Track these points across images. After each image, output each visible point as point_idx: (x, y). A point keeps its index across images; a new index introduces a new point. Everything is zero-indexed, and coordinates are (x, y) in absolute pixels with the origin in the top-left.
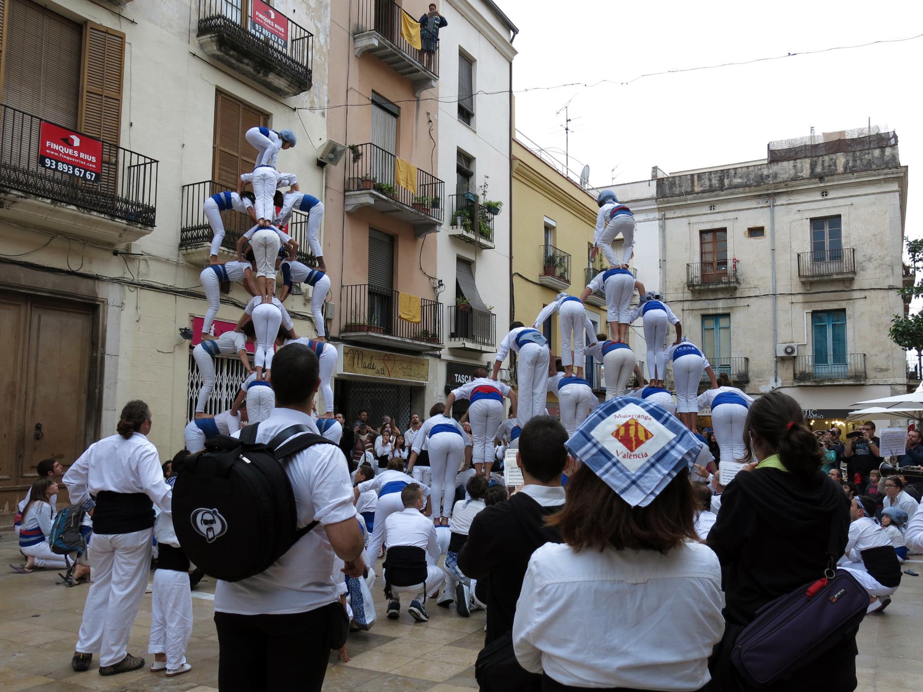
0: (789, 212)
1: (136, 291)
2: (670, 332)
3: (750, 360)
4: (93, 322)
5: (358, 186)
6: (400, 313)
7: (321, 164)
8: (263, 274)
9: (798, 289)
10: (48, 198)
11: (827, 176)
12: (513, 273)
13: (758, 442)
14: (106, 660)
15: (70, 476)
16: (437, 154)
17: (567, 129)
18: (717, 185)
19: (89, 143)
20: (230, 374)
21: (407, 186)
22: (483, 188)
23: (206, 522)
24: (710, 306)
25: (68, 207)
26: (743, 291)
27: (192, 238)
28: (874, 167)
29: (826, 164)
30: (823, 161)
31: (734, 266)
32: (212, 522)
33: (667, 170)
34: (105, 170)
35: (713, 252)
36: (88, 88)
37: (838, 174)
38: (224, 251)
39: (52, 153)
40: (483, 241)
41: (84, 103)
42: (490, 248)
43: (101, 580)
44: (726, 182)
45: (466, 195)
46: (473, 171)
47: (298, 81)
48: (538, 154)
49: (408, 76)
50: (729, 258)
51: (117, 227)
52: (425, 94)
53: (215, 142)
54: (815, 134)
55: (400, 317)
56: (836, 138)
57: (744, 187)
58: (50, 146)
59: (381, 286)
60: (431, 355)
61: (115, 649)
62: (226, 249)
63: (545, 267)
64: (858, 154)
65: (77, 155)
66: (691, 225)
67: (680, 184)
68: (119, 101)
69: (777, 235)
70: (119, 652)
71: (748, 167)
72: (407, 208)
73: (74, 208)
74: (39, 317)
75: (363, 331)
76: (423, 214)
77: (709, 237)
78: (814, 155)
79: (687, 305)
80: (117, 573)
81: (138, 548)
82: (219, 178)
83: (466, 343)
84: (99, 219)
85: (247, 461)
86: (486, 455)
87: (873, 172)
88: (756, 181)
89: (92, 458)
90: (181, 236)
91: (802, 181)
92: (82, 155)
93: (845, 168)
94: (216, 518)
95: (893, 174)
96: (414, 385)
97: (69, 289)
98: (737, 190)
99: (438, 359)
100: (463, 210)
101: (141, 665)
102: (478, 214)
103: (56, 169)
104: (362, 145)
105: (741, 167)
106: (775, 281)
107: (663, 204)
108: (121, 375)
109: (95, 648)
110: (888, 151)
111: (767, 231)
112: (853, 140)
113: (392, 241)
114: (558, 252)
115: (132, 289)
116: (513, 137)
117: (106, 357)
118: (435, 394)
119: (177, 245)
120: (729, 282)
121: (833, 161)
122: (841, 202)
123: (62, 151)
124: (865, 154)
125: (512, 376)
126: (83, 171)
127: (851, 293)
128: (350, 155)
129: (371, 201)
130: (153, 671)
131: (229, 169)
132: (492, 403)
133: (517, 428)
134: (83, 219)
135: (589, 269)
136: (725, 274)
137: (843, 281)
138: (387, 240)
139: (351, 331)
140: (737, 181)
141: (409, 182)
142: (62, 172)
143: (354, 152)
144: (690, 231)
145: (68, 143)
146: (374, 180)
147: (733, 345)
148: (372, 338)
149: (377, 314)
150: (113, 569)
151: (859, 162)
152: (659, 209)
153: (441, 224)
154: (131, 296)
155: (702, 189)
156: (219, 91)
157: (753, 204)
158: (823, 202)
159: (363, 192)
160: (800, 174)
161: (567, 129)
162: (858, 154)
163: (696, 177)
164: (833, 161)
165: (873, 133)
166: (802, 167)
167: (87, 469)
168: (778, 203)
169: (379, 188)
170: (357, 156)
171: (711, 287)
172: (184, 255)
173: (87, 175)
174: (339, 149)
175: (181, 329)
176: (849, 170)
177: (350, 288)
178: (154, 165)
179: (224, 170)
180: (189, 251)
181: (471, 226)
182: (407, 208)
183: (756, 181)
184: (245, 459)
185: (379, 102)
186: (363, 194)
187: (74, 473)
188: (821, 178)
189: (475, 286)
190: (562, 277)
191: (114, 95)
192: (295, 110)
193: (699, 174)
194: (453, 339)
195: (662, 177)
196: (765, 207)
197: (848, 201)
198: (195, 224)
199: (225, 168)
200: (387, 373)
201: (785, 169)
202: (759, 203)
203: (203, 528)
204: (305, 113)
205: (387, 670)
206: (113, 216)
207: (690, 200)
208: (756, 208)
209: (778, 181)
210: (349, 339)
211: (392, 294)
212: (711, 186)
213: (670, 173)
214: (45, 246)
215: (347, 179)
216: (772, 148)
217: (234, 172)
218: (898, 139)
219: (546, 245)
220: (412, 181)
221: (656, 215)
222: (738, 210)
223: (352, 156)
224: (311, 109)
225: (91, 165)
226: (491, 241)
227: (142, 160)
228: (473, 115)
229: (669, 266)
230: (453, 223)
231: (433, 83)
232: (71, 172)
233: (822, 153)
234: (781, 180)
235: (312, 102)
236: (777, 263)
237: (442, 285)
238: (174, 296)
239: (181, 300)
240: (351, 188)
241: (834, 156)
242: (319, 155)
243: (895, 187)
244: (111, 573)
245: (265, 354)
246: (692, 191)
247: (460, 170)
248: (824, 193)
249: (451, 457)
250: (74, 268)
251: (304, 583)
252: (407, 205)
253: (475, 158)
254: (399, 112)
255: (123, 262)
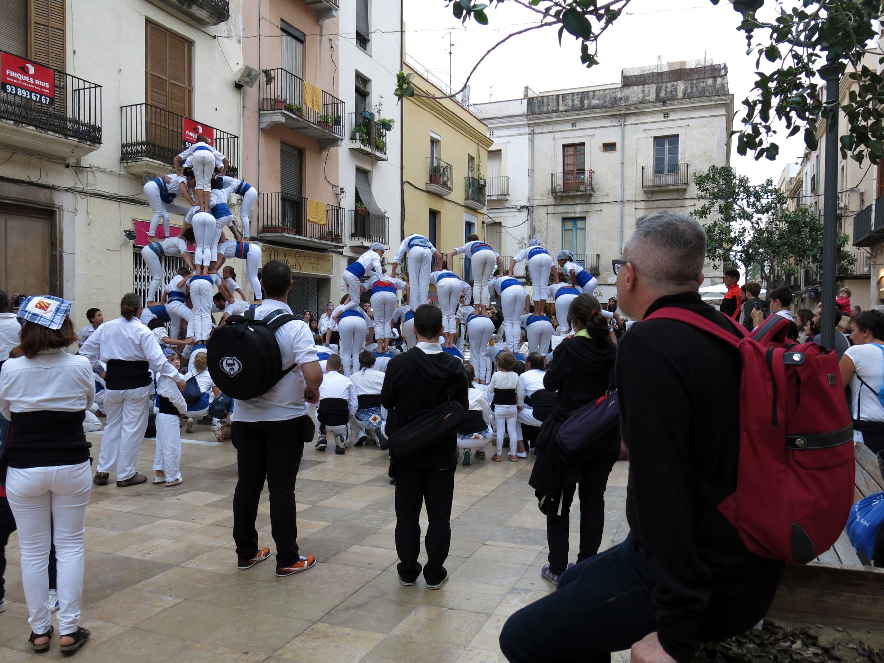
0: (636, 130)
1: (86, 199)
2: (536, 232)
3: (601, 256)
4: (51, 225)
5: (271, 106)
6: (309, 217)
7: (238, 86)
8: (201, 188)
9: (641, 197)
10: (11, 120)
11: (669, 100)
12: (404, 181)
13: (576, 323)
14: (122, 477)
15: (85, 349)
16: (338, 76)
17: (450, 53)
18: (579, 105)
19: (43, 71)
20: (167, 269)
21: (313, 106)
22: (378, 106)
23: (229, 365)
24: (570, 210)
25: (28, 127)
26: (597, 197)
27: (132, 153)
28: (707, 94)
29: (669, 90)
30: (666, 87)
31: (591, 176)
32: (233, 365)
33: (537, 90)
34: (57, 94)
35: (574, 164)
36: (35, 19)
37: (678, 99)
38: (160, 164)
39: (12, 80)
40: (378, 154)
41: (33, 33)
42: (385, 160)
43: (113, 423)
44: (586, 102)
45: (364, 114)
46: (369, 91)
47: (217, 13)
48: (425, 75)
49: (312, 6)
50: (586, 169)
51: (70, 144)
52: (327, 23)
53: (146, 67)
54: (662, 64)
55: (309, 220)
56: (678, 67)
57: (601, 107)
58: (9, 74)
59: (292, 192)
60: (335, 252)
61: (129, 468)
62: (162, 163)
63: (431, 176)
64: (695, 82)
65: (33, 82)
66: (556, 139)
67: (547, 103)
68: (63, 31)
69: (626, 151)
70: (131, 471)
71: (604, 90)
72: (314, 125)
73: (33, 128)
74: (6, 220)
75: (278, 232)
76: (327, 131)
77: (571, 151)
78: (659, 81)
79: (550, 209)
80: (127, 417)
81: (142, 399)
82: (152, 100)
83: (364, 242)
84: (54, 137)
85: (253, 330)
86: (385, 333)
87: (706, 98)
88: (610, 103)
89: (103, 336)
90: (122, 151)
91: (649, 104)
92: (37, 82)
93: (684, 94)
94: (235, 362)
95: (722, 100)
96: (321, 277)
97: (30, 198)
98: (595, 110)
99: (341, 256)
100: (360, 126)
101: (145, 481)
102: (374, 130)
103: (16, 95)
104: (273, 70)
105: (599, 90)
106: (623, 189)
107: (532, 120)
108: (78, 270)
109: (112, 469)
110: (719, 80)
111: (618, 146)
112: (691, 70)
113: (300, 154)
114: (442, 163)
115: (83, 197)
116: (404, 61)
117: (65, 255)
118: (338, 285)
119: (119, 159)
120: (586, 190)
121: (675, 87)
122: (679, 123)
123: (20, 78)
124: (700, 83)
125: (403, 269)
126: (39, 96)
127: (684, 201)
128: (263, 78)
129: (283, 120)
130: (155, 484)
131: (159, 91)
132: (388, 294)
133: (411, 312)
134: (41, 138)
135: (469, 178)
136: (583, 183)
137: (677, 191)
138: (296, 153)
139: (268, 232)
140: (595, 102)
141: (315, 102)
142: (21, 97)
143: (267, 76)
144: (555, 144)
145: (25, 71)
146: (285, 100)
147: (587, 243)
148: (285, 238)
149: (289, 218)
150: (123, 412)
151: (695, 89)
152: (529, 125)
153: (342, 140)
154: (82, 203)
155: (566, 108)
156: (148, 21)
157: (607, 123)
158: (665, 123)
159: (276, 111)
160: (647, 98)
161: (450, 53)
162: (695, 82)
163: (561, 97)
164: (675, 87)
165: (708, 64)
166: (649, 91)
167: (99, 344)
168: (628, 122)
169: (289, 108)
170: (270, 79)
171: (571, 194)
172: (125, 167)
173: (33, 96)
174: (254, 73)
175: (125, 231)
176: (687, 96)
177: (266, 195)
178: (98, 89)
179: (155, 92)
180: (130, 164)
181: (367, 141)
182: (314, 125)
183: (610, 103)
184: (251, 328)
185: (287, 30)
186: (276, 113)
187: (88, 347)
188: (664, 102)
189: (371, 193)
190: (445, 184)
191: (59, 26)
192: (214, 37)
193: (563, 94)
194: (353, 238)
195: (532, 96)
196: (618, 126)
197: (685, 123)
198: (134, 140)
199: (156, 90)
200: (298, 268)
201: (635, 93)
202: (612, 122)
203: (227, 369)
204: (224, 42)
205: (321, 479)
206: (66, 135)
207: (556, 118)
208: (610, 126)
209: (629, 103)
210: (267, 239)
211: (301, 200)
212: (573, 105)
213: (540, 93)
214: (8, 160)
215: (261, 99)
216: (626, 74)
217: (164, 93)
218: (728, 70)
219: (432, 157)
220: (317, 102)
221: (527, 130)
222: (596, 128)
223: (265, 79)
224: (229, 37)
225: (45, 90)
226: (385, 154)
227: (87, 85)
228: (369, 41)
229: (537, 175)
230: (353, 138)
231: (334, 13)
232: (29, 97)
233: (665, 80)
234: (631, 102)
235: (229, 30)
236: (626, 174)
237: (343, 192)
238: (118, 203)
239: (124, 206)
240: (265, 108)
241: (675, 83)
242: (237, 79)
243: (723, 112)
244: (122, 416)
245: (203, 252)
246: (557, 110)
247: (358, 91)
248: (666, 115)
249: (356, 335)
250: (34, 179)
251: (288, 403)
252: (313, 123)
253: (371, 80)
254: (305, 38)
255: (74, 174)
